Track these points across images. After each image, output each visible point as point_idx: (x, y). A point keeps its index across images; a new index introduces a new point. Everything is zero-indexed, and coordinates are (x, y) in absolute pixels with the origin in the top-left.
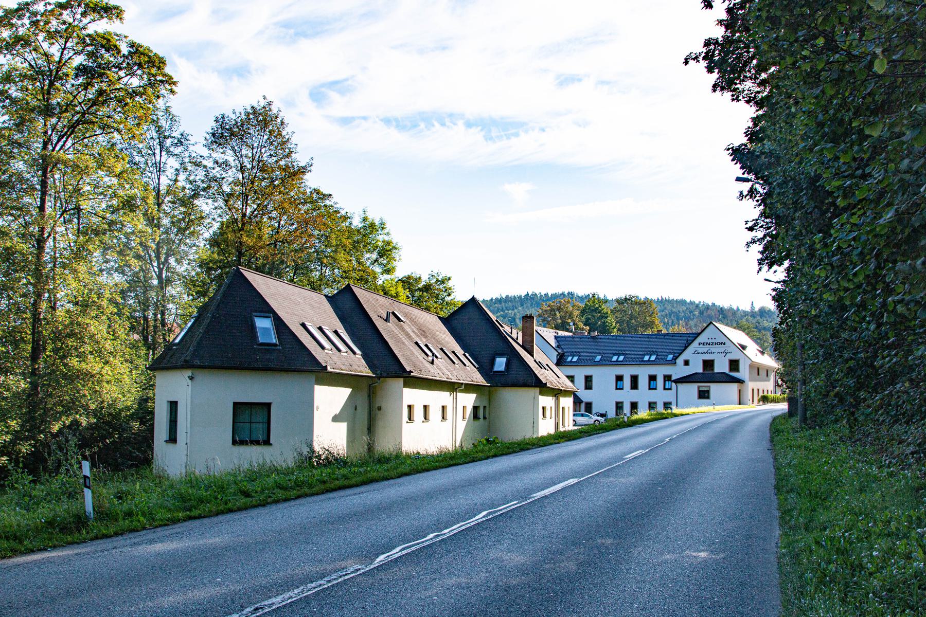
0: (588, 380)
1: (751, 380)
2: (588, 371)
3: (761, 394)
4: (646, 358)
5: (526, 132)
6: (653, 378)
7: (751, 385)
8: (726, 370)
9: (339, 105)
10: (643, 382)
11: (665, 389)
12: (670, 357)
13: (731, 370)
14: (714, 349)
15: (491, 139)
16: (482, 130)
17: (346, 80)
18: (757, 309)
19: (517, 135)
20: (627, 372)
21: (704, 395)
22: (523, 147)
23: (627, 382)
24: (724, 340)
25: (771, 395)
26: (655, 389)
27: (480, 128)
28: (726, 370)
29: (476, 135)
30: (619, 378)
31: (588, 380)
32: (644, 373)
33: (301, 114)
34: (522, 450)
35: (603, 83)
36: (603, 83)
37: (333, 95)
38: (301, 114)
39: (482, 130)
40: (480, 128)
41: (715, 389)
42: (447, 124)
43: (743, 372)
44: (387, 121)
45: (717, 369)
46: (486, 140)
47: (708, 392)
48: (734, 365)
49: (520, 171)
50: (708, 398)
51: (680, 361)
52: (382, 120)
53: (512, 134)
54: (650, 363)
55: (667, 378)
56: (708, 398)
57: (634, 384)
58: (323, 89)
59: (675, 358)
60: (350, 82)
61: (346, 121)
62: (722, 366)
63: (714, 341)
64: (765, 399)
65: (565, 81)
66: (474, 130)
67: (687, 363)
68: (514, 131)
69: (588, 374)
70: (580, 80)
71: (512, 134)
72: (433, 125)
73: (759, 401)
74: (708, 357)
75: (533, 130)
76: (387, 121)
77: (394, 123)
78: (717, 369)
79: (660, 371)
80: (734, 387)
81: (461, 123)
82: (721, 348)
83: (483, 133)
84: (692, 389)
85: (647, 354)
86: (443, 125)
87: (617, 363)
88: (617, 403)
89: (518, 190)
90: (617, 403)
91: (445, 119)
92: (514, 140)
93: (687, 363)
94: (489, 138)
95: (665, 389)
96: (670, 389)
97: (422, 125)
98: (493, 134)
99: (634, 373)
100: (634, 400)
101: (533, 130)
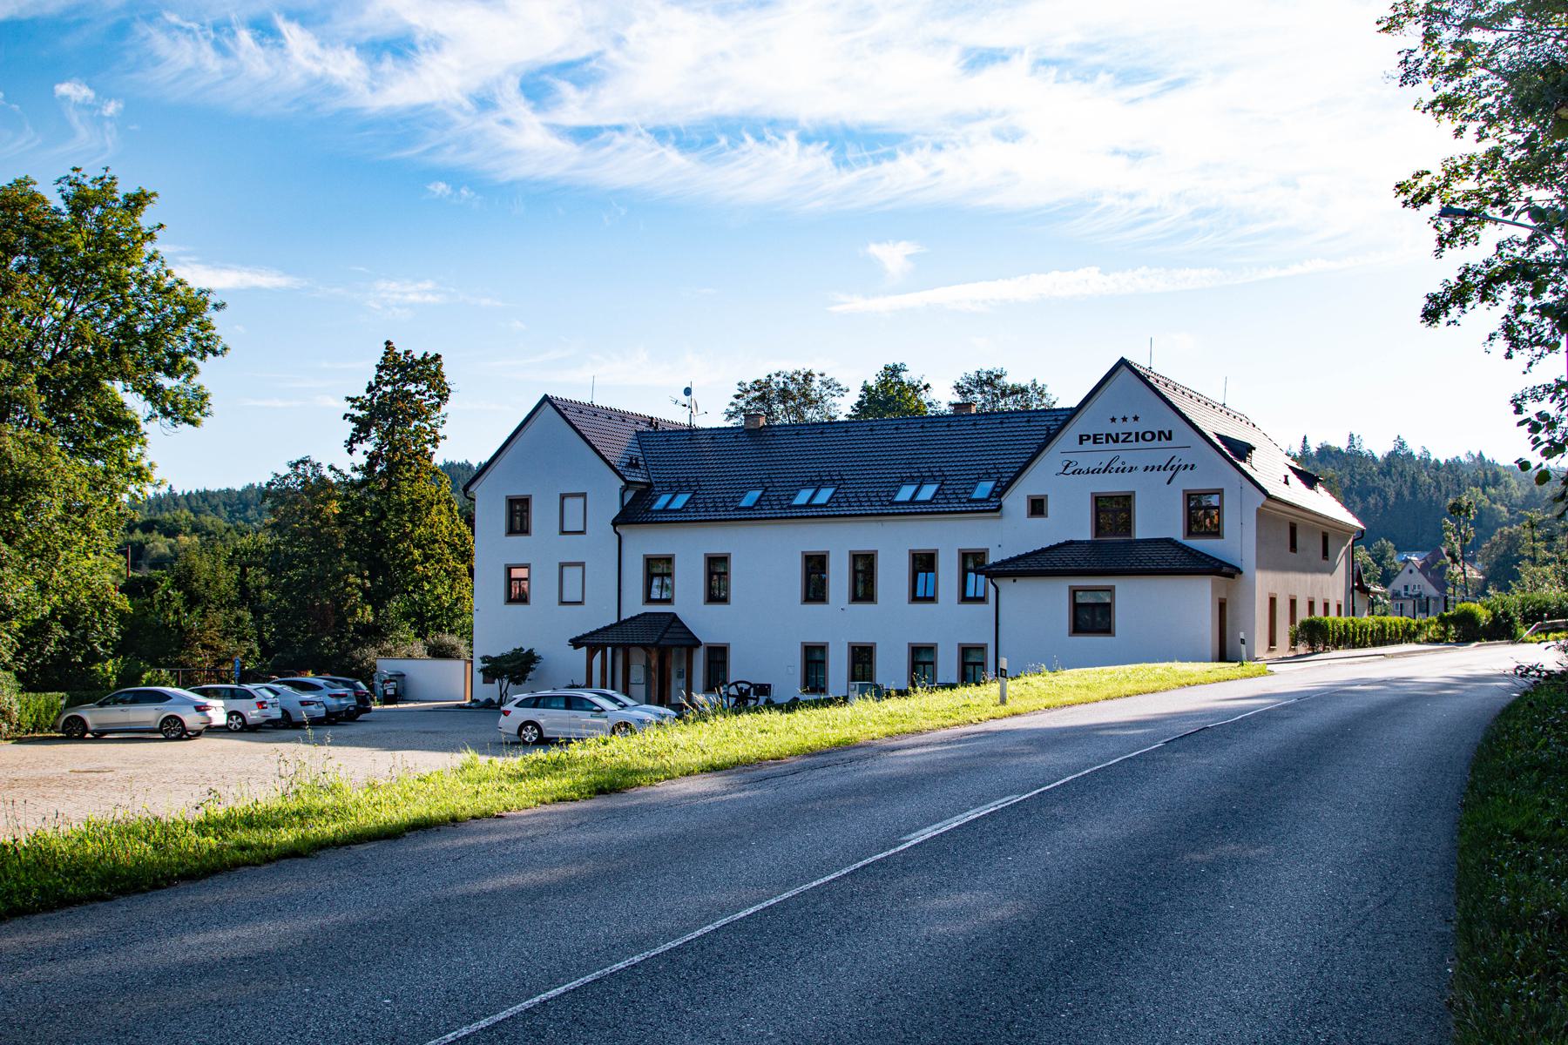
0: (717, 567)
1: (1264, 564)
2: (717, 540)
3: (1302, 615)
4: (905, 493)
5: (910, 150)
6: (924, 562)
7: (1264, 584)
8: (1177, 532)
9: (575, 109)
10: (893, 576)
11: (964, 599)
12: (984, 489)
13: (1190, 533)
14: (1131, 455)
15: (846, 163)
16: (829, 148)
17: (588, 59)
18: (1313, 450)
19: (892, 157)
20: (839, 542)
21: (1092, 619)
22: (905, 174)
23: (839, 578)
24: (1171, 423)
25: (617, 133)
26: (932, 599)
27: (826, 144)
28: (1177, 532)
29: (818, 159)
30: (815, 566)
31: (717, 567)
32: (893, 544)
33: (507, 122)
34: (156, 886)
35: (1047, 63)
36: (1047, 63)
37: (566, 89)
38: (507, 122)
39: (829, 148)
40: (826, 144)
41: (1132, 598)
42: (769, 137)
43: (1238, 538)
44: (660, 134)
45: (1143, 529)
46: (837, 165)
47: (1107, 609)
48: (1202, 513)
49: (899, 220)
50: (1107, 630)
51: (1016, 501)
52: (650, 132)
53: (883, 156)
54: (914, 509)
55: (973, 562)
56: (1107, 630)
57: (864, 585)
58: (546, 78)
59: (1001, 490)
60: (593, 64)
61: (584, 134)
62: (1158, 519)
63: (1131, 427)
64: (1314, 636)
65: (980, 59)
66: (811, 149)
67: (1037, 507)
68: (885, 149)
69: (717, 549)
70: (1005, 59)
71: (883, 156)
72: (743, 140)
73: (1294, 642)
74: (1112, 485)
75: (921, 147)
76: (660, 134)
77: (673, 137)
78: (1143, 529)
79: (949, 538)
80: (1199, 594)
81: (791, 136)
82: (1158, 453)
83: (830, 154)
84: (1049, 601)
85: (911, 480)
86: (760, 139)
87: (812, 513)
88: (916, 650)
89: (893, 255)
90: (916, 650)
91: (766, 128)
92: (887, 166)
93: (1037, 507)
94: (841, 163)
95: (964, 599)
96: (982, 600)
97: (723, 141)
98: (850, 156)
99: (863, 546)
100: (862, 638)
101: (921, 147)
